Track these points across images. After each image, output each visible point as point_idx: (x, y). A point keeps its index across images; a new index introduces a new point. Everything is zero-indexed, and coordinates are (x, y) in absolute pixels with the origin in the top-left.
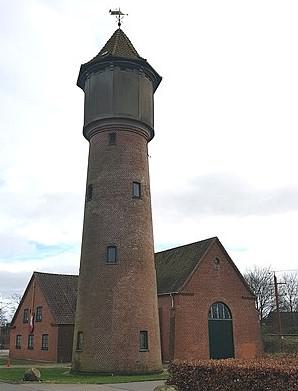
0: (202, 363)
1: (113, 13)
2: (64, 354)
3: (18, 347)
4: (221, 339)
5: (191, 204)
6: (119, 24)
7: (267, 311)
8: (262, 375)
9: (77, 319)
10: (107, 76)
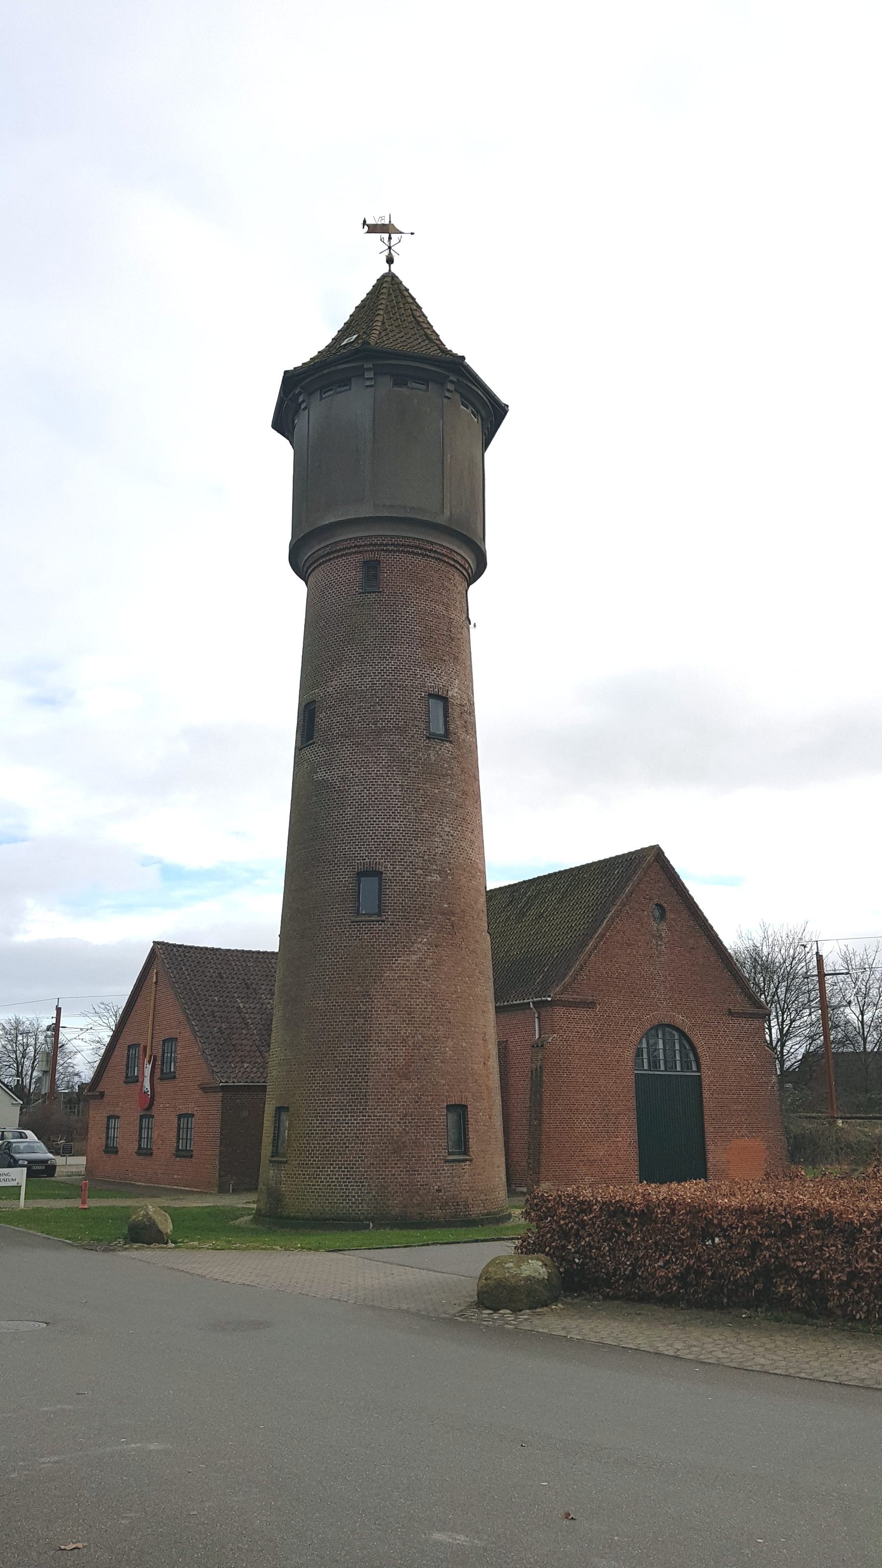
0: (617, 1193)
1: (373, 229)
2: (238, 1167)
3: (110, 1150)
4: (671, 1131)
5: (581, 758)
6: (390, 260)
7: (796, 1049)
8: (784, 1226)
9: (274, 1072)
10: (357, 403)
